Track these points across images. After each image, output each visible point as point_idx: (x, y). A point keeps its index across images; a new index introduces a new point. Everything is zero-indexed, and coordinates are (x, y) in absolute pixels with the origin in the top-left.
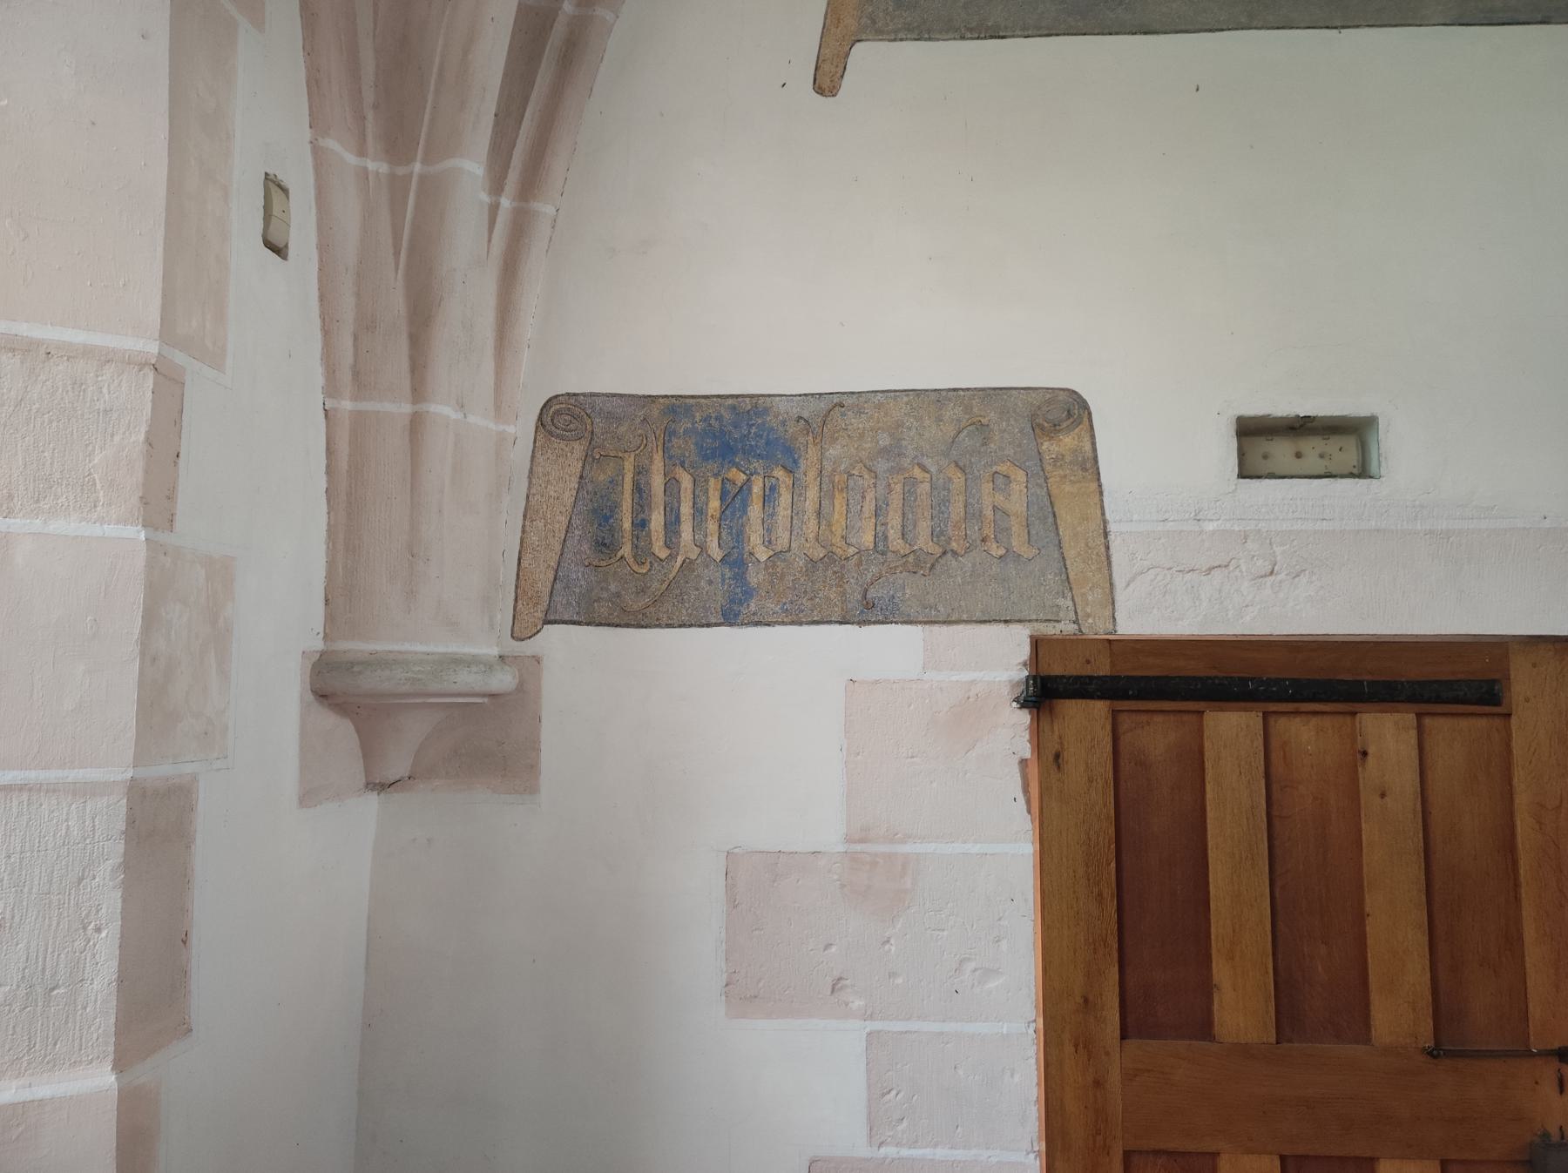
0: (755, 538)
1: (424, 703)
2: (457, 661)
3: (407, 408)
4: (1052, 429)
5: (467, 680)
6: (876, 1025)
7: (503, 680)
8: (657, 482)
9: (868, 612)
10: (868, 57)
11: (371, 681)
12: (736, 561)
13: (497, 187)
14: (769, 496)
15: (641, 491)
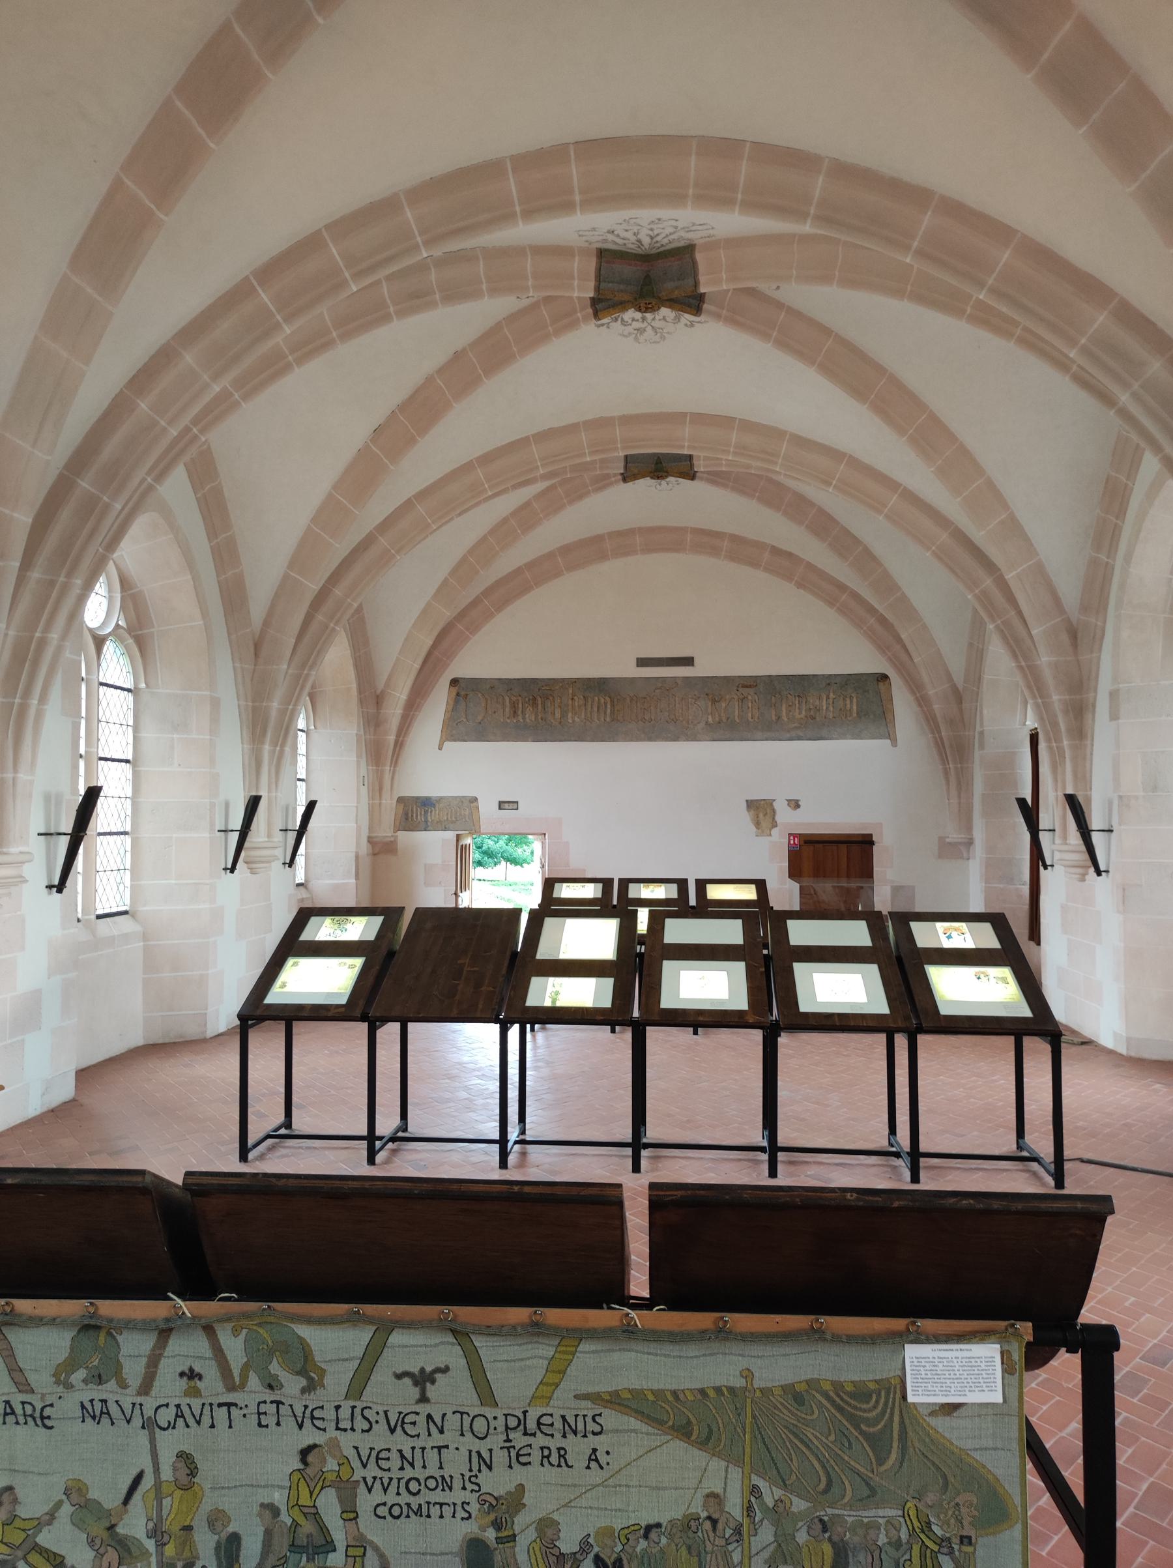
0: (429, 818)
1: (79, 737)
2: (387, 837)
3: (378, 802)
4: (472, 802)
5: (389, 839)
6: (1137, 1512)
7: (392, 839)
8: (415, 810)
9: (445, 829)
10: (447, 744)
11: (375, 840)
12: (426, 821)
13: (391, 766)
14: (431, 812)
15: (412, 811)
